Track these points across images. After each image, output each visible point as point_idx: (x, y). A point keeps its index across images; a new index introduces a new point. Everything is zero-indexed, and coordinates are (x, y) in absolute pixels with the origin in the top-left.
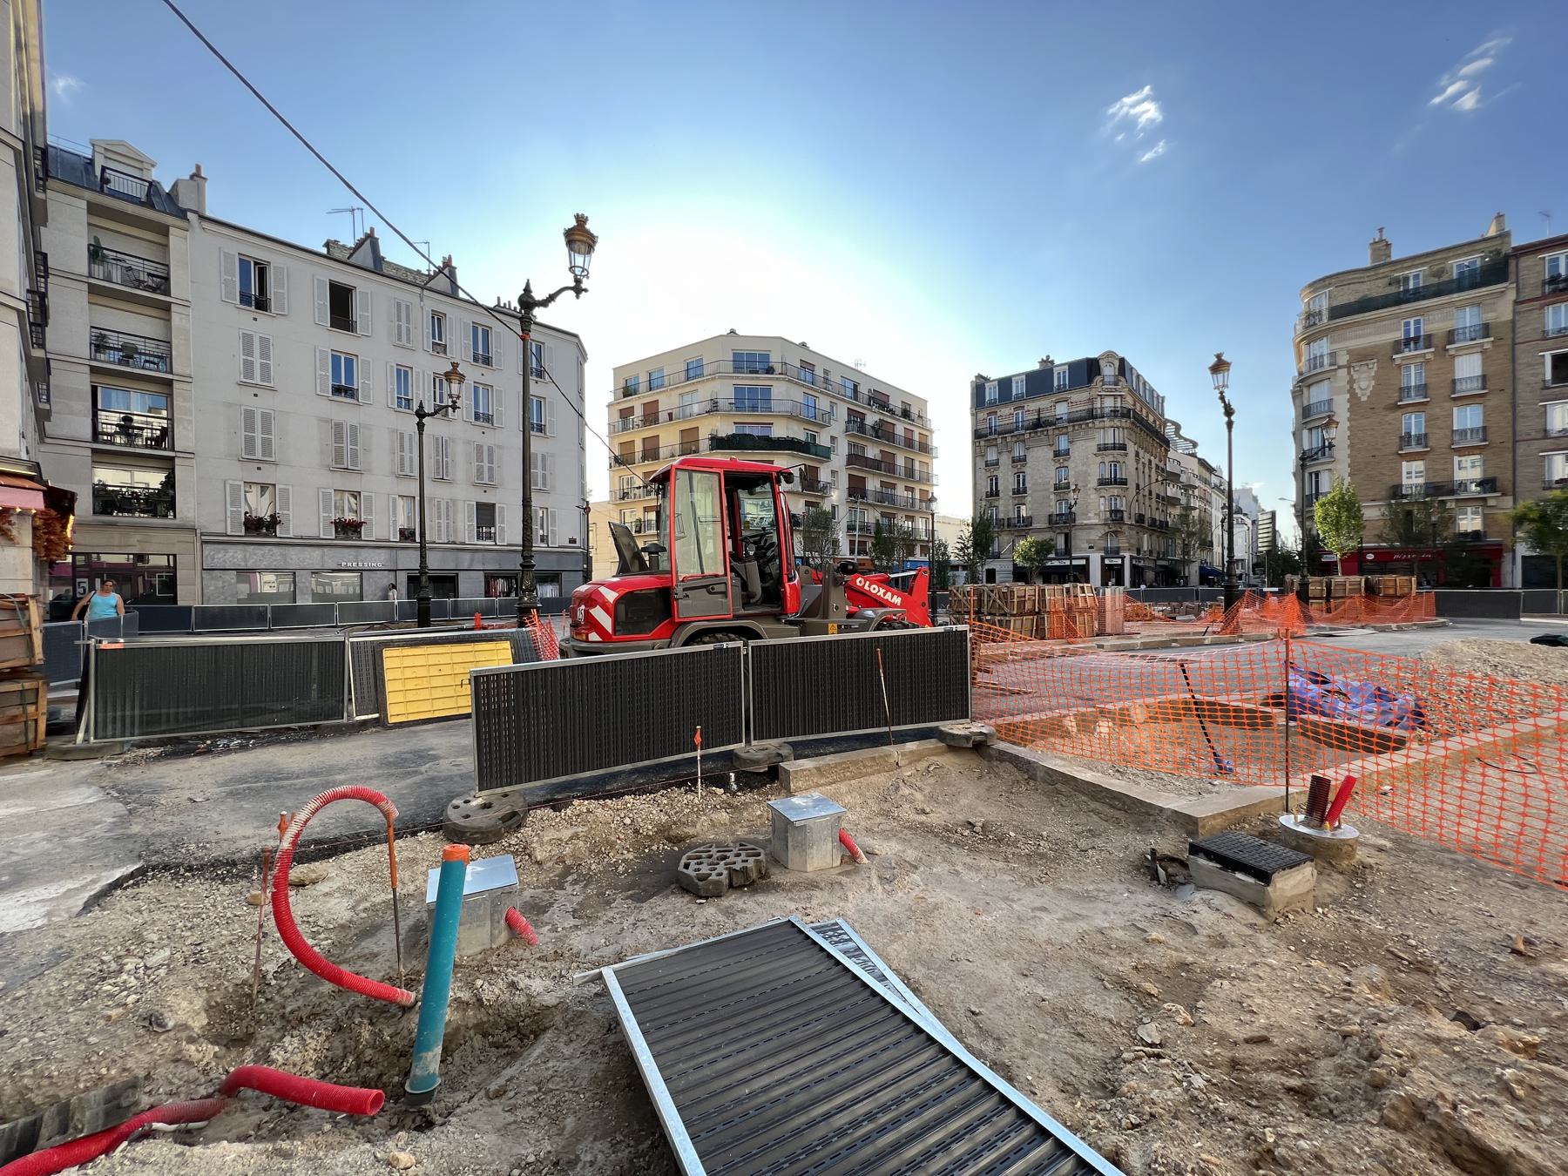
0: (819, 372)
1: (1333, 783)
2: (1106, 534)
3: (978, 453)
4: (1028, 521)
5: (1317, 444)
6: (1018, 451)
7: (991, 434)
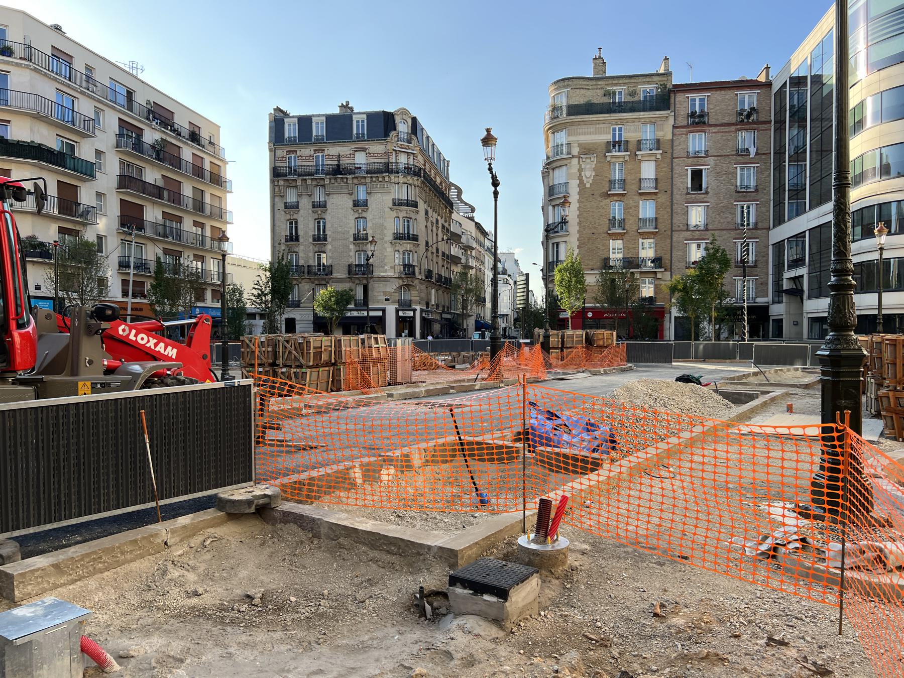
0: (79, 65)
1: (554, 503)
2: (400, 287)
3: (276, 194)
4: (328, 270)
5: (558, 219)
6: (319, 196)
7: (290, 174)
